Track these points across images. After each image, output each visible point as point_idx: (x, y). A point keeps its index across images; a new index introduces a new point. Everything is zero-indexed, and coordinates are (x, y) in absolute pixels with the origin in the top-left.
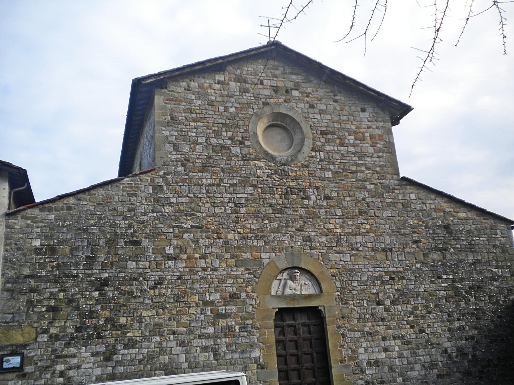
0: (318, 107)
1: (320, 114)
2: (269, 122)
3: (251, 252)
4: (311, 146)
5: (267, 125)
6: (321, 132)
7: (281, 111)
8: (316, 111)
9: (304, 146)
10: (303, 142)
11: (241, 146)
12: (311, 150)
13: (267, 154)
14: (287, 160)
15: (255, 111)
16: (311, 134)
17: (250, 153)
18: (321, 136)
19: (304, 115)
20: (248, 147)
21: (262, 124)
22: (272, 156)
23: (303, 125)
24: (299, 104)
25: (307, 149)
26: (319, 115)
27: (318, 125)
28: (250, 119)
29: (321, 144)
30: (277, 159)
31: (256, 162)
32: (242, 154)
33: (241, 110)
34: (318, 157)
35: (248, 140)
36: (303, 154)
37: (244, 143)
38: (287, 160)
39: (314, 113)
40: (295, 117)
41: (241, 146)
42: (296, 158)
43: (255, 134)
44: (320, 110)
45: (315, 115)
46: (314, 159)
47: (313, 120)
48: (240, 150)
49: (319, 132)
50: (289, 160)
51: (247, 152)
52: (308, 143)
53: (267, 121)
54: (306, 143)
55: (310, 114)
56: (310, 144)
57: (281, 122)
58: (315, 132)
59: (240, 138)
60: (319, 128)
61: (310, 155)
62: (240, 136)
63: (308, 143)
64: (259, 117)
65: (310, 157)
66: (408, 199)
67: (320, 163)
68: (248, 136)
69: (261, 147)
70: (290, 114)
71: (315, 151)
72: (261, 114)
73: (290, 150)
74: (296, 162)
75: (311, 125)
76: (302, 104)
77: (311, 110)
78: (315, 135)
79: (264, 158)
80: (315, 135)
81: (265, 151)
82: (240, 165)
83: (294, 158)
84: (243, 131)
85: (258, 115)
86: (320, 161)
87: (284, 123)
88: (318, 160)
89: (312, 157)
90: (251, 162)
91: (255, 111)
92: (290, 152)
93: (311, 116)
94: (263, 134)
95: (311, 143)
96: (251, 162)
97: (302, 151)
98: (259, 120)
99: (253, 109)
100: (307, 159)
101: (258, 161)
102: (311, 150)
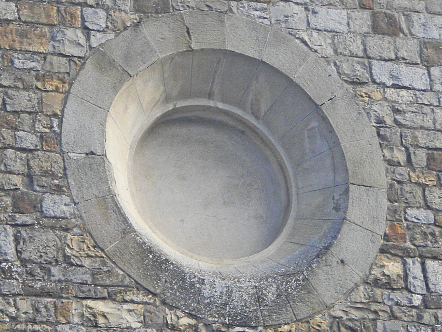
0: (417, 30)
1: (428, 65)
2: (167, 99)
3: (370, 274)
4: (382, 228)
5: (158, 113)
6: (430, 158)
7: (230, 46)
8: (409, 48)
9: (345, 228)
10: (340, 208)
11: (21, 218)
12: (382, 251)
13: (157, 263)
14: (259, 299)
15: (97, 40)
16: (383, 165)
17: (66, 258)
18: (430, 179)
19: (346, 68)
20: (61, 225)
21: (133, 109)
22: (179, 274)
23: (342, 117)
24: (322, 11)
25: (358, 245)
26: (421, 71)
27: (418, 120)
28: (67, 79)
29: (431, 215)
30: (207, 291)
31: (100, 306)
32: (24, 262)
33: (23, 35)
34: (418, 284)
35: (58, 190)
36: (337, 270)
37: (37, 207)
38: (259, 299)
39: (397, 59)
40: (299, 75)
41: (21, 218)
42: (306, 287)
43: (96, 158)
44: (424, 44)
45: (403, 68)
46: (397, 296)
47: (391, 93)
48: (17, 240)
49: (420, 157)
50: (271, 296)
51: (52, 253)
52: (367, 211)
53: (158, 95)
54: (354, 212)
55: (376, 66)
56: (375, 219)
57: (224, 101)
58: (401, 157)
59: (17, 180)
60: (423, 138)
61: (376, 272)
62: (19, 166)
63: (367, 211)
64: (117, 71)
65: (376, 283)
66: (184, 327)
67: (427, 317)
68: (58, 169)
69: (127, 228)
70: (277, 58)
71: (404, 255)
72: (127, 57)
73: (272, 249)
74: (303, 310)
75: (380, 121)
76: (333, 12)
77: (380, 45)
78: (403, 171)
79: (139, 287)
80: (403, 171)
81: (145, 251)
82: (14, 319)
83: (295, 282)
84: (30, 140)
85: (112, 63)
86: (426, 305)
87: (240, 104)
88: (417, 300)
89: (389, 285)
90: (75, 307)
91: (97, 40)
92: (275, 255)
93: (381, 72)
94: (137, 153)
95: (383, 214)
96: (75, 307)
97: (337, 252)
98: (115, 90)
99: (87, 30)
100: (361, 295)
101: (111, 297)
102: (382, 251)
